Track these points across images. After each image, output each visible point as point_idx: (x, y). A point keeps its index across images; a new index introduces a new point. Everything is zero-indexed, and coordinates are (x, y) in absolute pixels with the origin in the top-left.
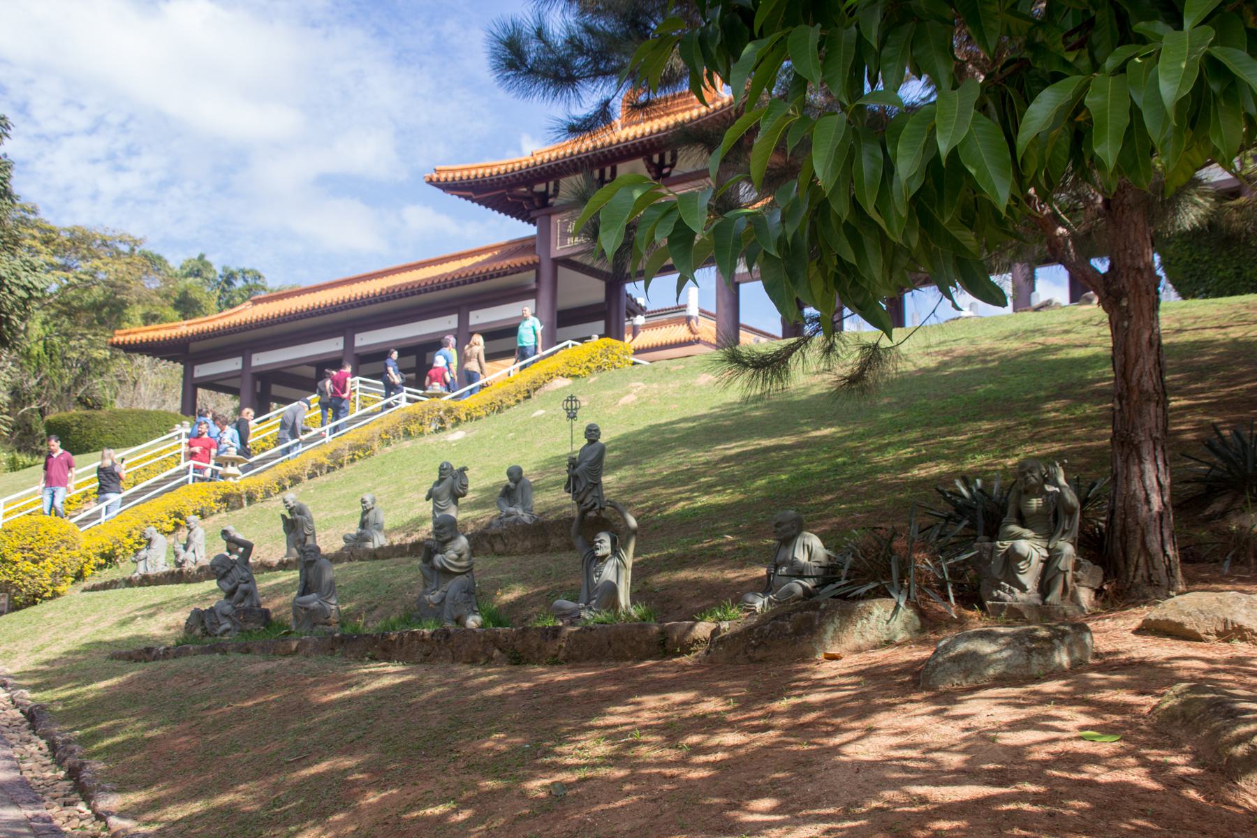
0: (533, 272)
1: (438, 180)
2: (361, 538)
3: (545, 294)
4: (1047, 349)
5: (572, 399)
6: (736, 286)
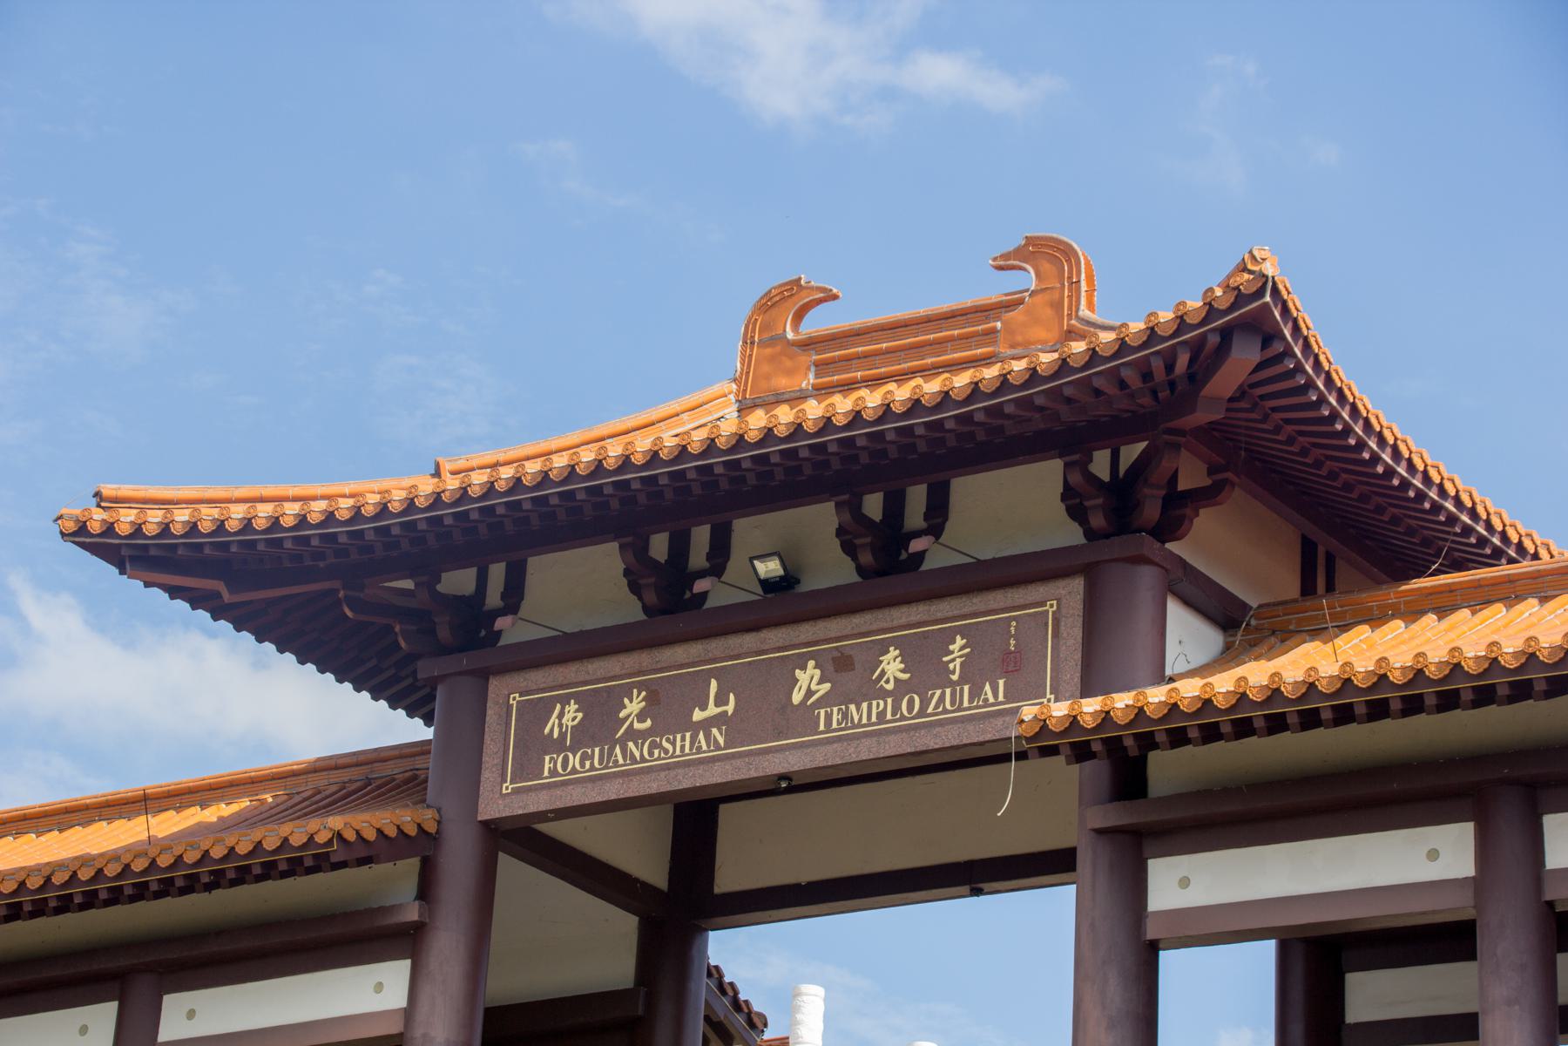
0: (411, 865)
1: (109, 530)
3: (447, 945)
6: (1149, 954)
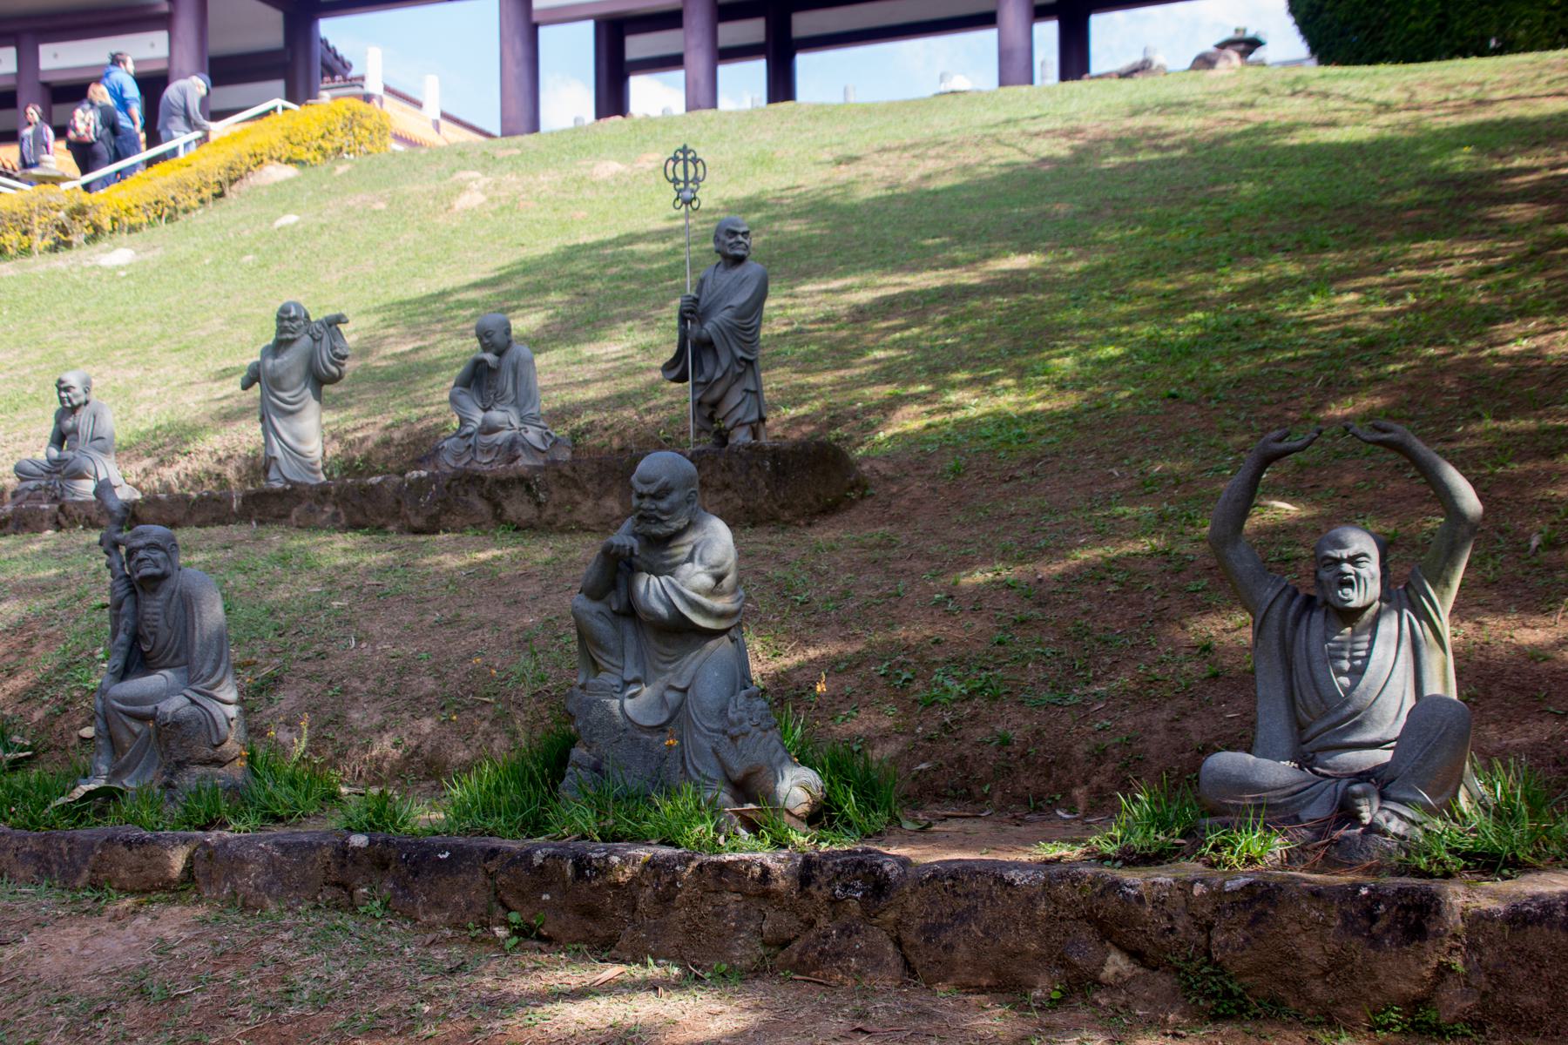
2: (63, 471)
4: (1261, 130)
5: (685, 155)
6: (533, 30)
